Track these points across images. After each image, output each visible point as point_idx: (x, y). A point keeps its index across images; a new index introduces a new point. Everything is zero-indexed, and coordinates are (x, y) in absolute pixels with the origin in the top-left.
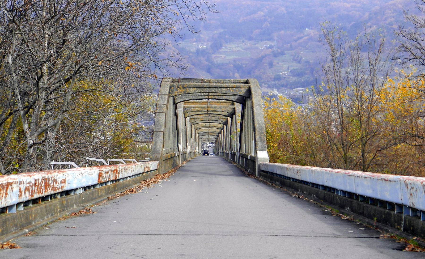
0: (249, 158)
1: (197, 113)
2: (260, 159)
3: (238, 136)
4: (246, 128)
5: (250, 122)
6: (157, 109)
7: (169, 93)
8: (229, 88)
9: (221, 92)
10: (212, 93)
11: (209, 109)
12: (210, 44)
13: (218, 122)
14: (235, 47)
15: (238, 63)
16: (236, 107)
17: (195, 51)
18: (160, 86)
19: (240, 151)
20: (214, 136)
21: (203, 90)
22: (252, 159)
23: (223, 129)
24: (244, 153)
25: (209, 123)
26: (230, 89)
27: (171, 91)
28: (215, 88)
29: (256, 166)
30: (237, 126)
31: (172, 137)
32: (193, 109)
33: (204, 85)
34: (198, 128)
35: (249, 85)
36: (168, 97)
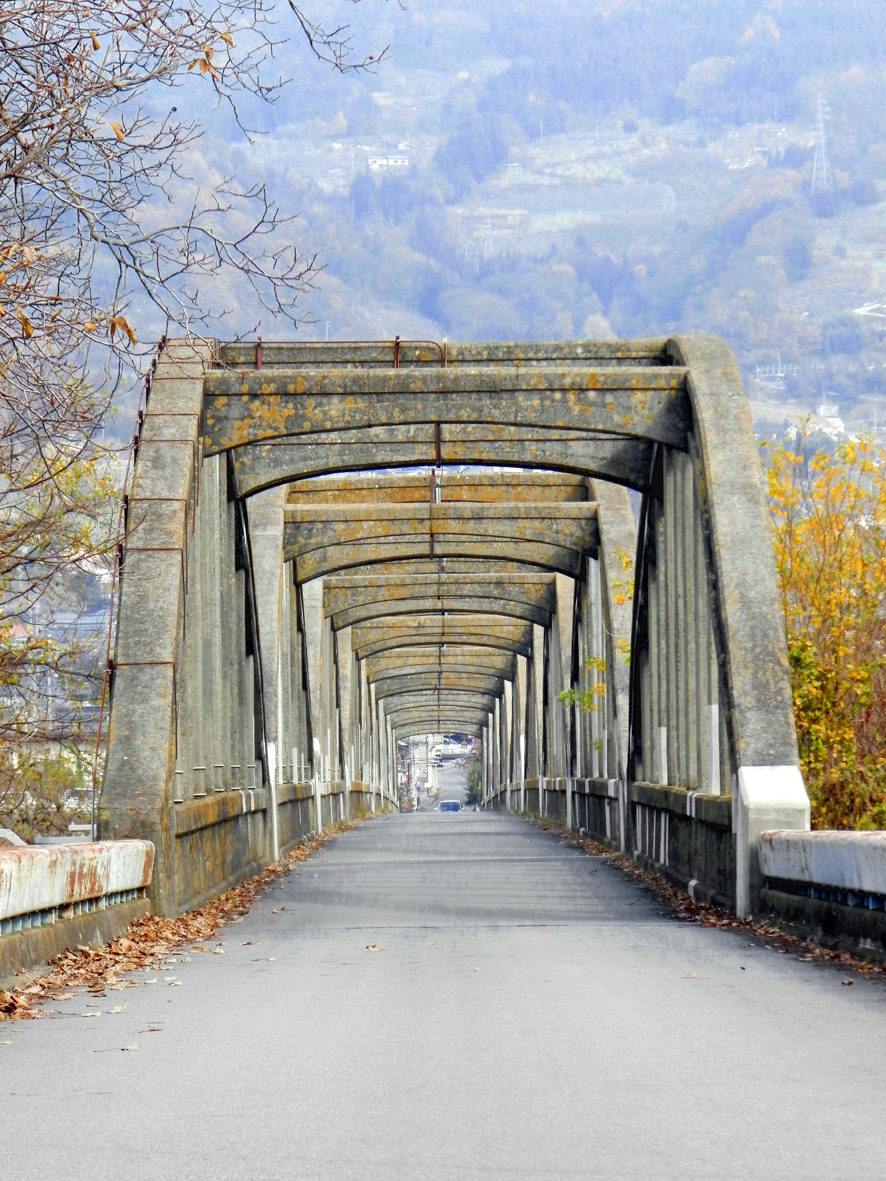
0: (691, 810)
1: (370, 552)
2: (760, 810)
3: (618, 687)
4: (667, 630)
5: (691, 599)
6: (132, 526)
7: (202, 428)
8: (563, 390)
9: (512, 419)
10: (459, 427)
11: (439, 526)
12: (432, 144)
13: (497, 606)
14: (586, 160)
15: (600, 254)
16: (602, 512)
17: (345, 192)
18: (148, 390)
19: (632, 776)
20: (473, 691)
21: (404, 410)
22: (711, 816)
23: (525, 647)
24: (658, 787)
25: (442, 612)
26: (564, 401)
27: (210, 422)
28: (474, 396)
29: (733, 860)
30: (615, 625)
31: (224, 698)
32: (342, 526)
33: (408, 376)
34: (375, 647)
35: (681, 370)
36: (195, 453)
